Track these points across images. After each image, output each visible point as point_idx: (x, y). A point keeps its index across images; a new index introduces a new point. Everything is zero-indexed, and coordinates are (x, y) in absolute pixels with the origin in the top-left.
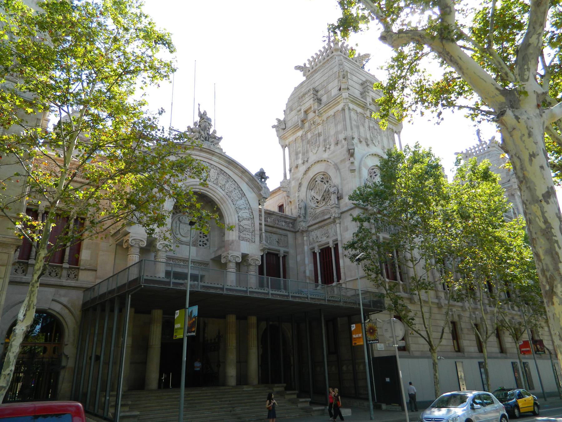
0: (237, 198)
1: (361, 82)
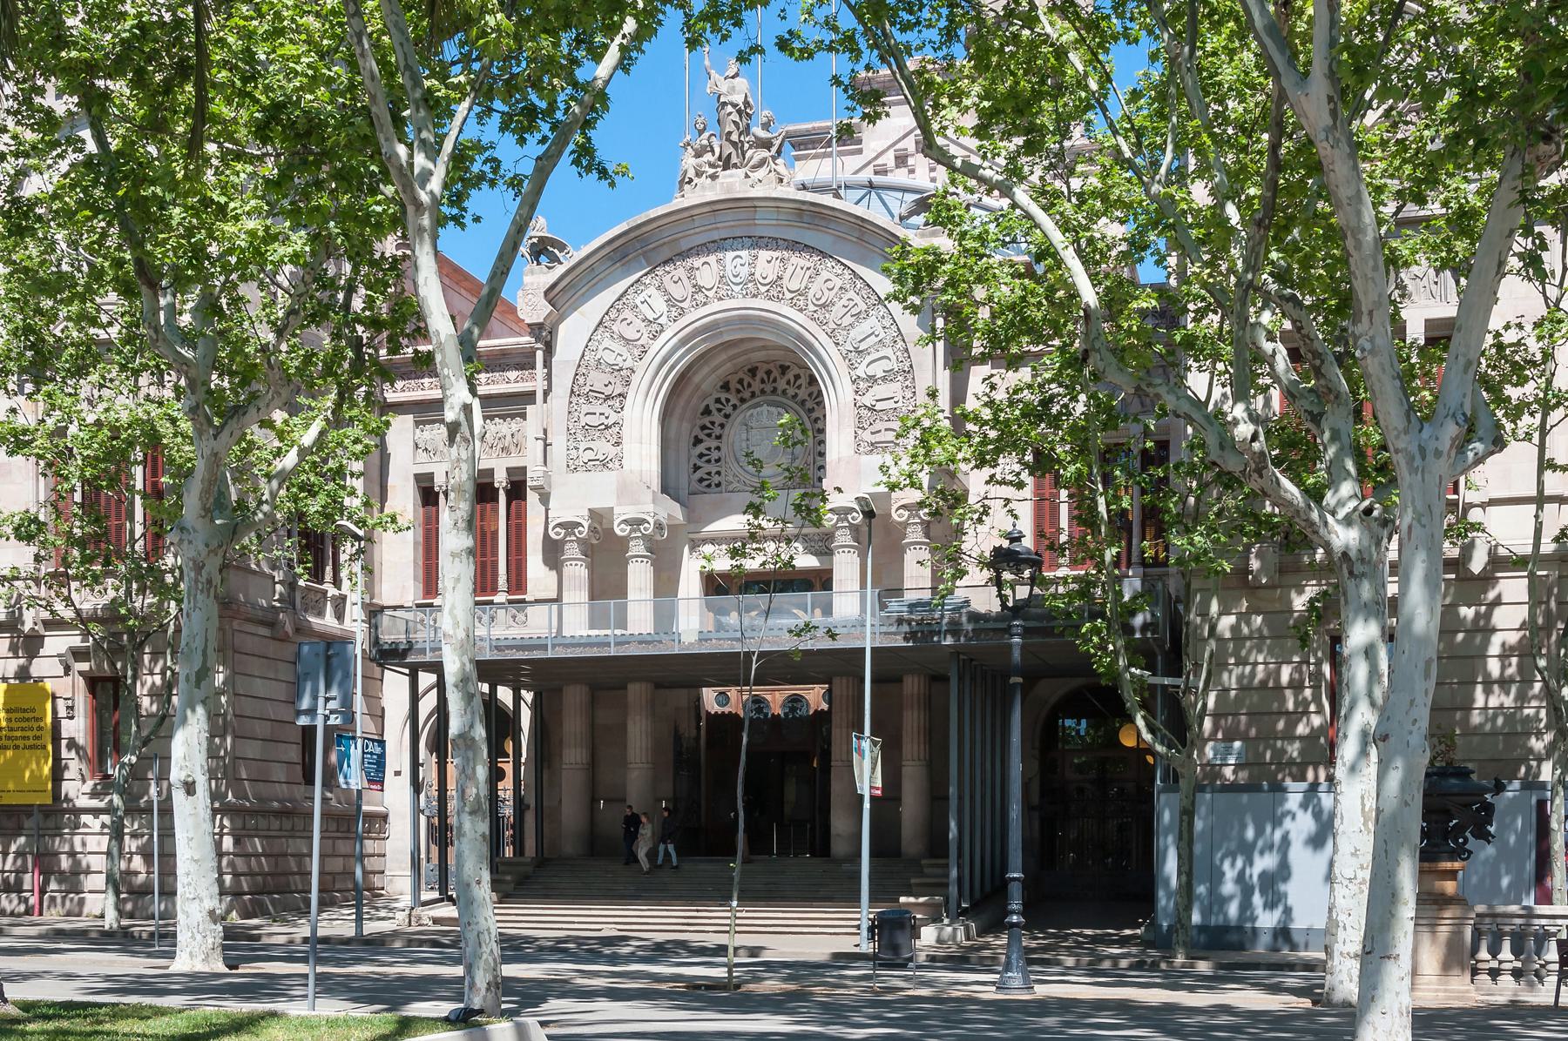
0: (848, 320)
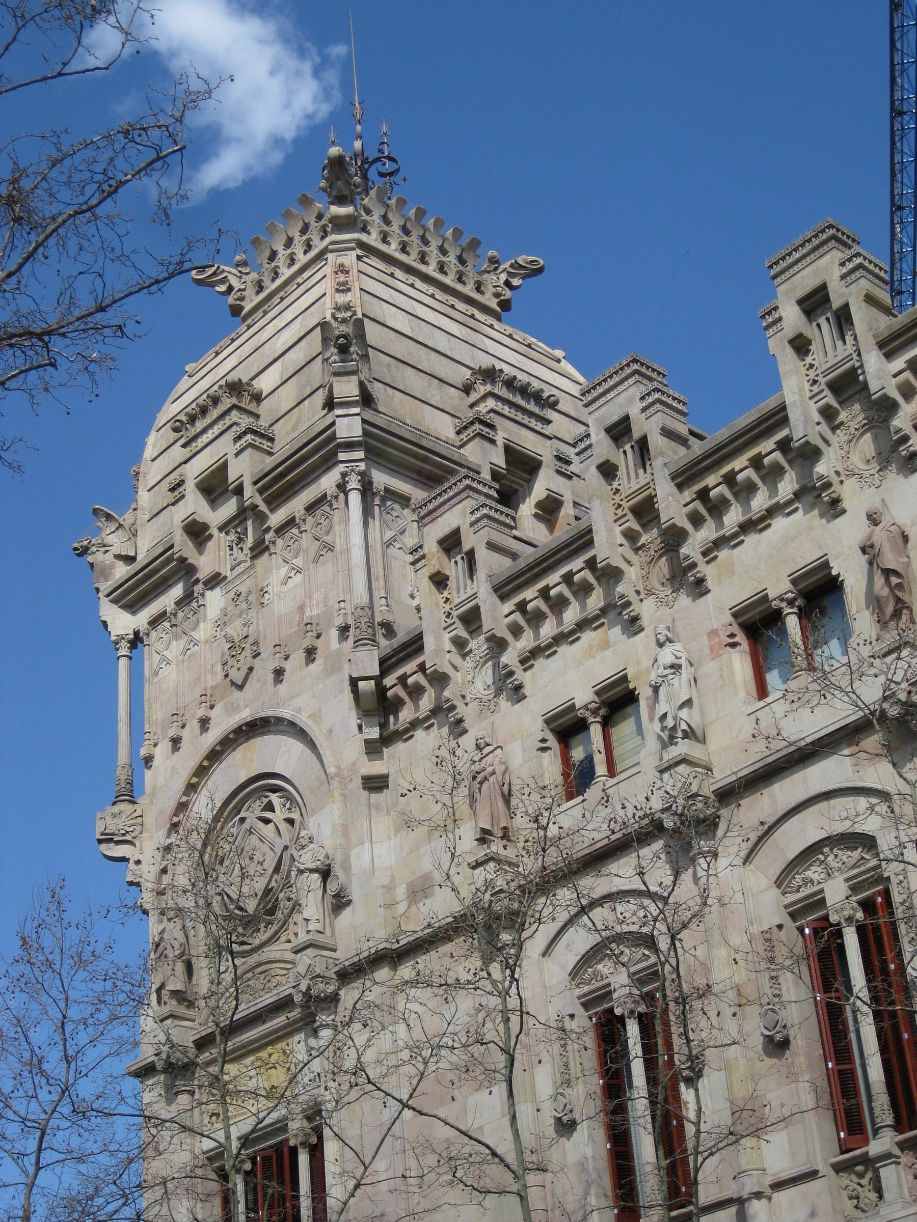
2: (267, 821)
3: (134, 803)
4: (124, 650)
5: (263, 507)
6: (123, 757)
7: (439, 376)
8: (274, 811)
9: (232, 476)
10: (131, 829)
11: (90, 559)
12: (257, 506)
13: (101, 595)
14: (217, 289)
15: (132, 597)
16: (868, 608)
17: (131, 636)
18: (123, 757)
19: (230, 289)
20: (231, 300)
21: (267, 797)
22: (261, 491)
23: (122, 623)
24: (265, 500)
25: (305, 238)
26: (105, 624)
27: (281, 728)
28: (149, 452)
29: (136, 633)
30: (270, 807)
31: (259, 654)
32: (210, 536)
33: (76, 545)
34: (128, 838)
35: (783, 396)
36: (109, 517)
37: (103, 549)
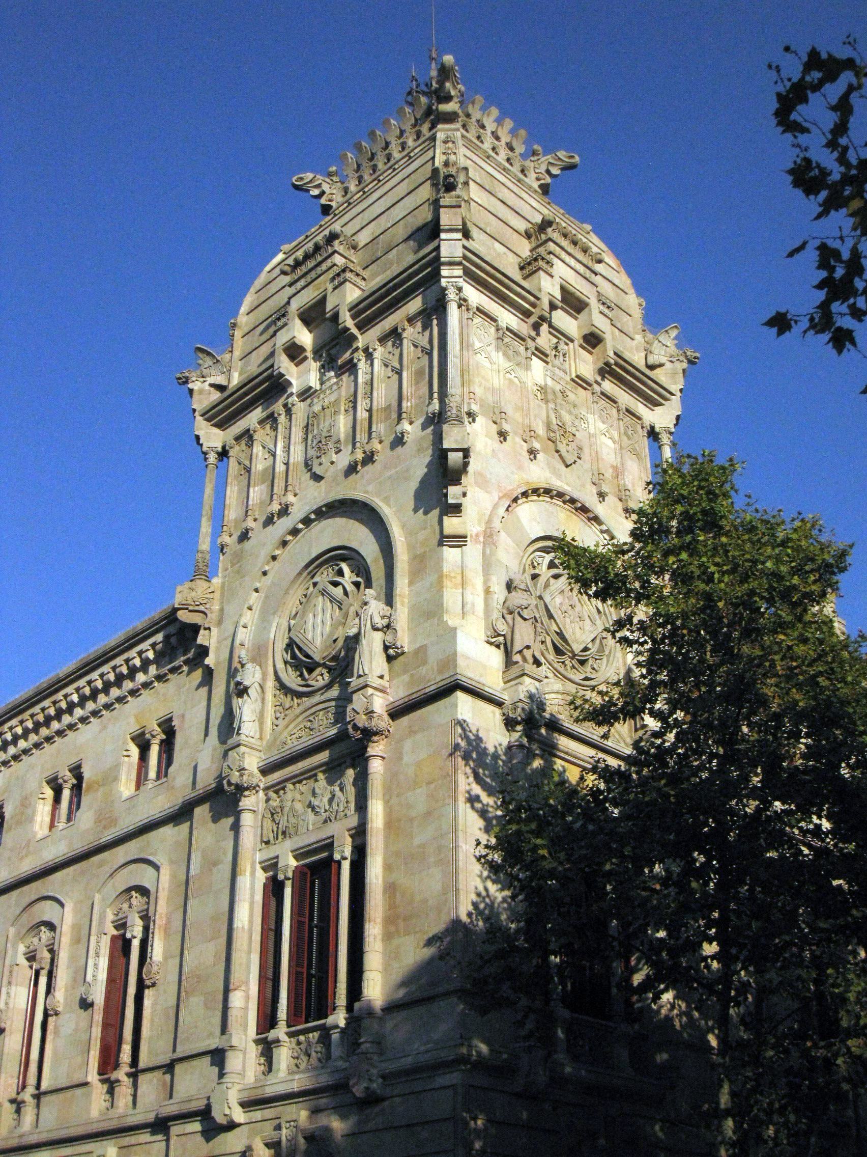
1: (522, 226)
2: (335, 584)
3: (209, 581)
4: (212, 458)
5: (354, 331)
6: (205, 544)
7: (520, 218)
8: (343, 576)
9: (329, 306)
10: (205, 601)
11: (190, 386)
12: (349, 329)
13: (197, 414)
14: (312, 193)
15: (223, 416)
16: (429, 942)
17: (220, 449)
18: (205, 544)
19: (323, 193)
20: (323, 201)
21: (337, 565)
22: (354, 317)
23: (213, 438)
24: (356, 325)
25: (399, 141)
26: (198, 438)
27: (355, 509)
28: (243, 309)
29: (224, 447)
30: (340, 573)
31: (340, 450)
32: (306, 358)
33: (178, 375)
34: (202, 608)
35: (106, 1152)
36: (208, 354)
37: (202, 380)
